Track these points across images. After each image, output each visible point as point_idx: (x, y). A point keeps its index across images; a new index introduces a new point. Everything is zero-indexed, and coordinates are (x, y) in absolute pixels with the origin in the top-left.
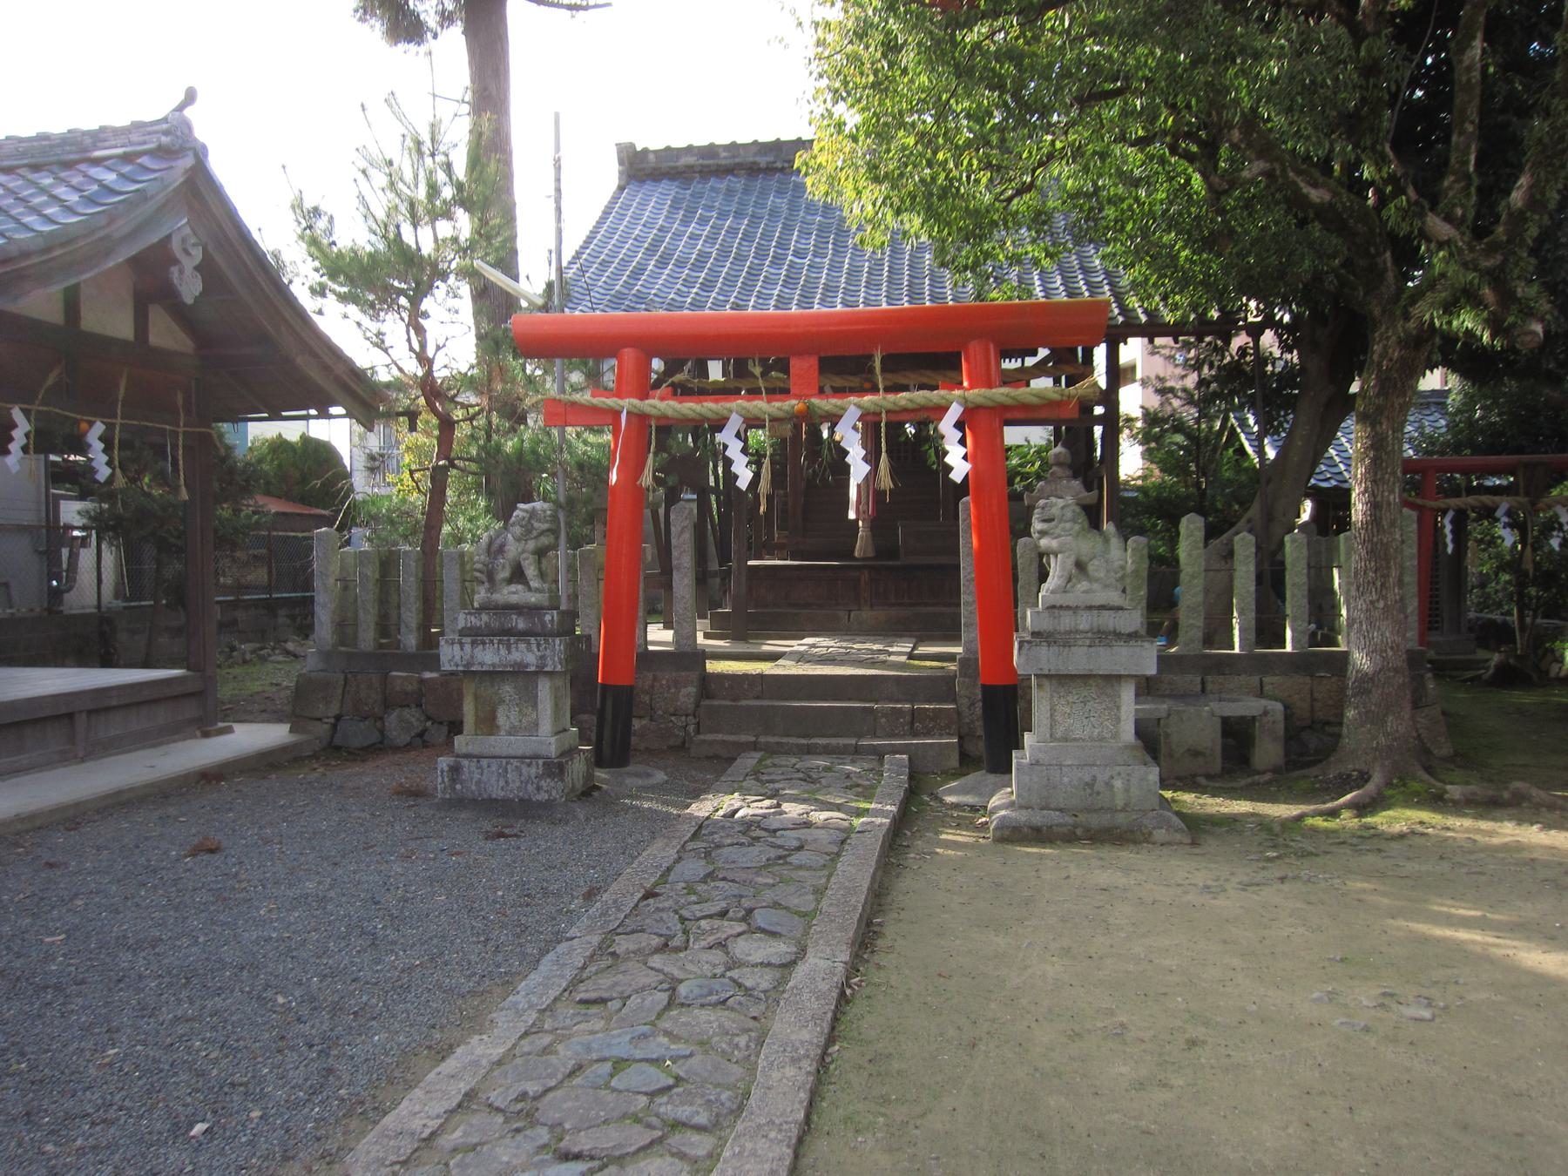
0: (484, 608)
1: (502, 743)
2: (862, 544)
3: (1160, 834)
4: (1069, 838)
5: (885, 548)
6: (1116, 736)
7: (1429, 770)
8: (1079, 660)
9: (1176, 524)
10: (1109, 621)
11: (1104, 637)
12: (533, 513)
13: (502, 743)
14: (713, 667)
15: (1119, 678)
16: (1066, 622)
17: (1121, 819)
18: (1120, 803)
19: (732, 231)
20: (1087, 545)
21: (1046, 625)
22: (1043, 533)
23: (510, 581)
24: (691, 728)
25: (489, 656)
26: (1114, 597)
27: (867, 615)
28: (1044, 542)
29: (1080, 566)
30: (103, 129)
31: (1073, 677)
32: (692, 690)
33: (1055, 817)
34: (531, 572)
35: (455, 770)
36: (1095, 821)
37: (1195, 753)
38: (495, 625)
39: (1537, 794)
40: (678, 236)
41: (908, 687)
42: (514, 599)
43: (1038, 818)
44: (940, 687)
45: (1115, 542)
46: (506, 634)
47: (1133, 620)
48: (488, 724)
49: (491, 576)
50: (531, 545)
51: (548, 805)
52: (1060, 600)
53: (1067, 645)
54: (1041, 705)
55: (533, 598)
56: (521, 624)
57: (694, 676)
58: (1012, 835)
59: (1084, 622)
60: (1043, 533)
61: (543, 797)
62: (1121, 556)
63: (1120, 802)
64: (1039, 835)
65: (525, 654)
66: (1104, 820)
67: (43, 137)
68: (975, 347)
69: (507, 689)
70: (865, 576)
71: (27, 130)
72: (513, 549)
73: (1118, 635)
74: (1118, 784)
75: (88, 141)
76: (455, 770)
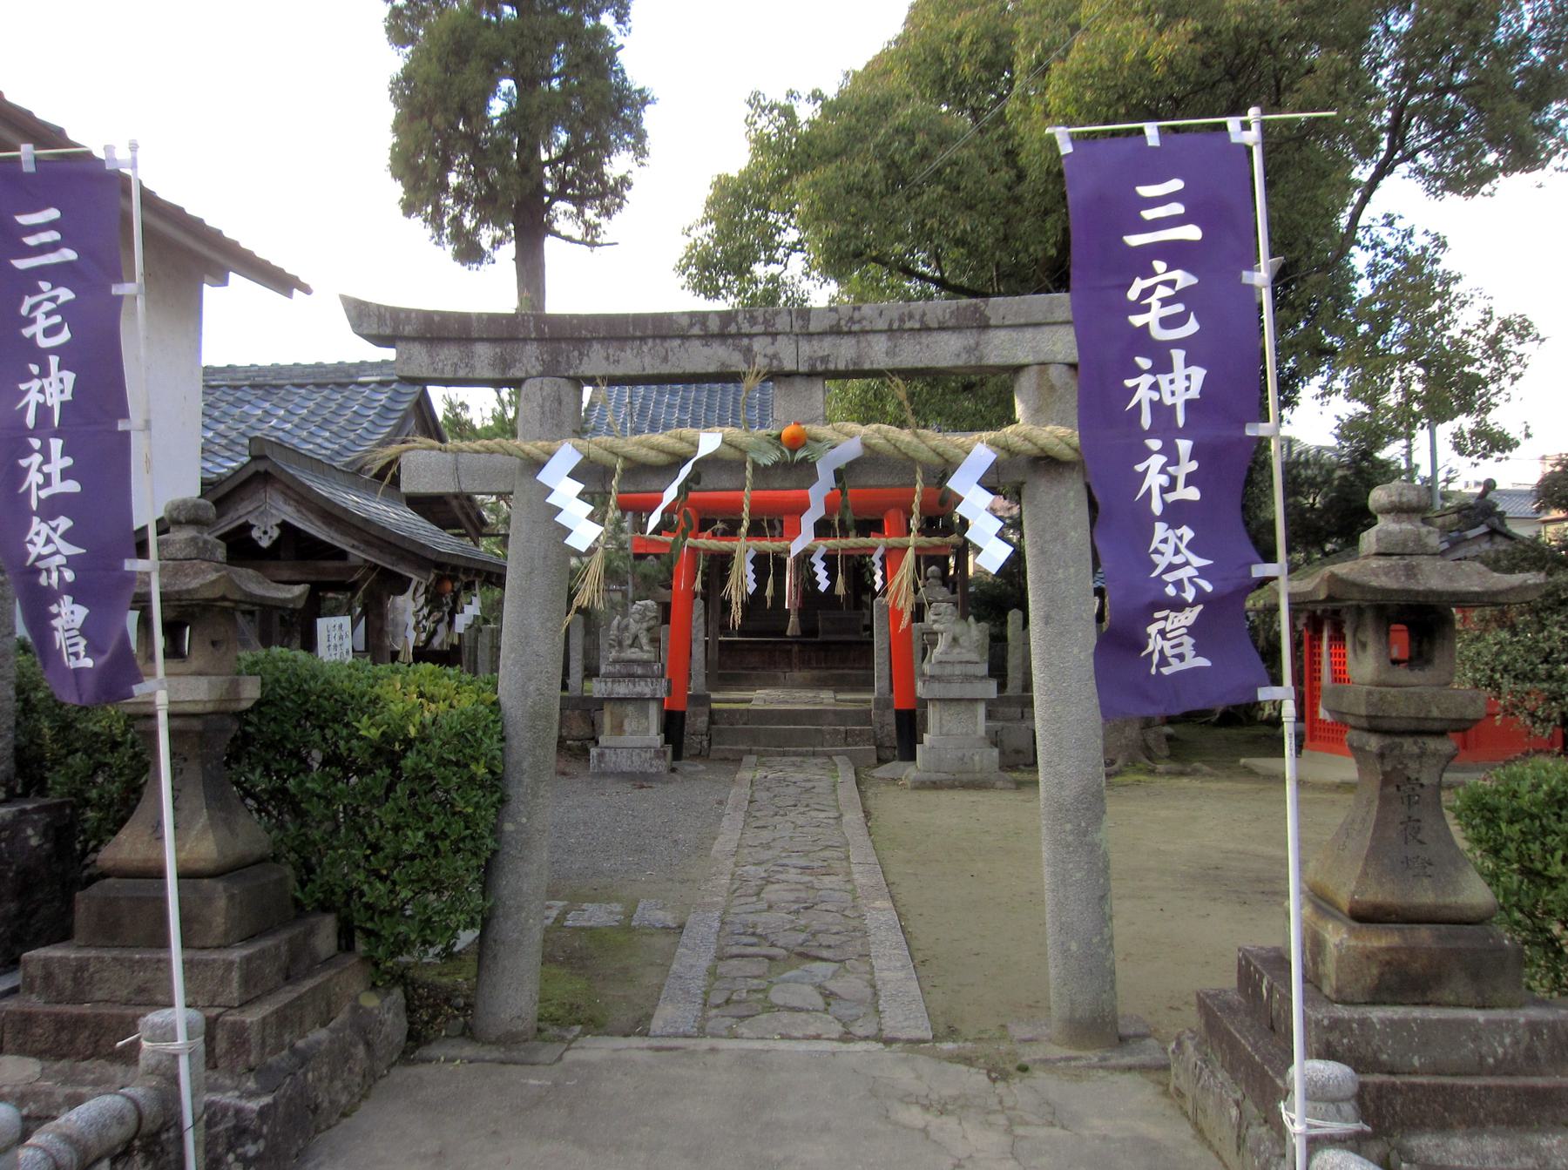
0: (615, 662)
1: (627, 740)
2: (793, 626)
3: (999, 784)
4: (952, 786)
5: (808, 629)
6: (975, 732)
7: (1149, 758)
8: (955, 691)
9: (1006, 615)
10: (971, 669)
11: (968, 678)
12: (646, 607)
13: (627, 740)
14: (714, 706)
15: (976, 700)
16: (948, 670)
17: (978, 776)
18: (977, 768)
19: (697, 402)
20: (959, 628)
21: (937, 671)
22: (935, 621)
23: (631, 646)
24: (705, 743)
25: (622, 689)
26: (974, 657)
27: (797, 675)
28: (936, 627)
29: (955, 640)
30: (363, 363)
31: (952, 700)
32: (705, 719)
33: (943, 776)
34: (644, 640)
35: (601, 755)
36: (965, 777)
37: (1018, 752)
38: (624, 671)
39: (1206, 768)
40: (657, 403)
41: (841, 716)
42: (634, 657)
43: (934, 777)
44: (864, 717)
45: (973, 626)
46: (631, 676)
47: (983, 669)
48: (619, 729)
49: (620, 644)
50: (645, 625)
51: (658, 774)
52: (944, 658)
53: (949, 682)
54: (933, 715)
55: (645, 656)
56: (640, 671)
57: (706, 710)
58: (921, 786)
59: (958, 670)
60: (935, 621)
61: (654, 770)
62: (975, 632)
63: (977, 768)
64: (935, 786)
65: (644, 688)
66: (970, 777)
67: (319, 366)
68: (892, 512)
69: (630, 709)
70: (796, 648)
71: (308, 359)
72: (634, 627)
73: (976, 677)
74: (977, 758)
75: (353, 371)
76: (601, 755)
